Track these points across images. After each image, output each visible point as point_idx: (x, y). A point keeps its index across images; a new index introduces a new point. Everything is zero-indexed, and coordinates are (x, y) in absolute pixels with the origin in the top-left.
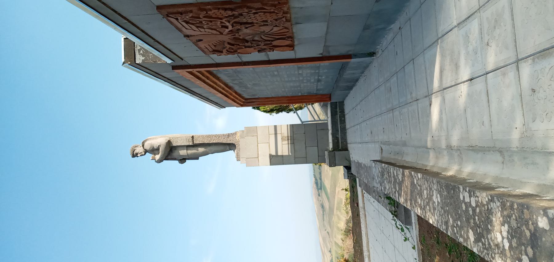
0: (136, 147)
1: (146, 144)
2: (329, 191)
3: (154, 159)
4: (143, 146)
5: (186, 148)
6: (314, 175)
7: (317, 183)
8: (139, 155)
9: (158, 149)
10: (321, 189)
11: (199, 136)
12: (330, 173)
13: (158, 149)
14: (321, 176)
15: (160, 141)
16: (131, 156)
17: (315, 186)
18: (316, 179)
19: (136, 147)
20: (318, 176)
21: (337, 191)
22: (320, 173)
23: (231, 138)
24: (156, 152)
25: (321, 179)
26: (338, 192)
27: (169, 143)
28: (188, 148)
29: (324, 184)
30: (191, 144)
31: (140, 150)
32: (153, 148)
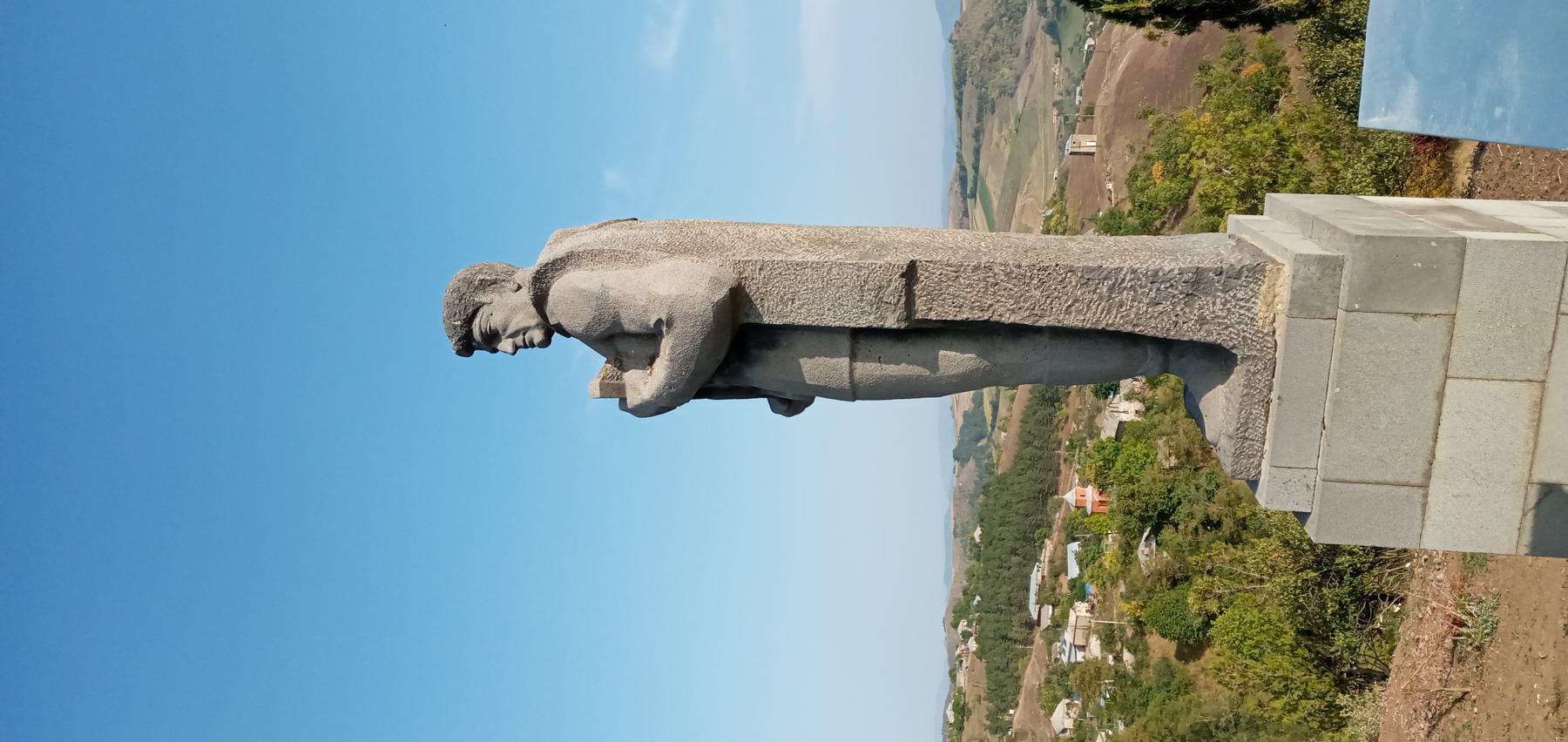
0: (484, 285)
1: (559, 289)
2: (995, 203)
3: (613, 390)
4: (540, 301)
5: (845, 343)
6: (959, 155)
7: (963, 180)
8: (506, 345)
9: (652, 336)
10: (974, 196)
11: (958, 270)
12: (1007, 152)
13: (652, 336)
14: (977, 160)
15: (676, 287)
16: (450, 346)
17: (957, 187)
18: (963, 169)
19: (484, 285)
20: (968, 160)
21: (1019, 205)
22: (977, 151)
23: (1210, 304)
24: (632, 348)
25: (976, 168)
26: (1023, 207)
27: (737, 299)
28: (864, 345)
29: (983, 182)
30: (891, 322)
31: (508, 308)
32: (616, 322)
